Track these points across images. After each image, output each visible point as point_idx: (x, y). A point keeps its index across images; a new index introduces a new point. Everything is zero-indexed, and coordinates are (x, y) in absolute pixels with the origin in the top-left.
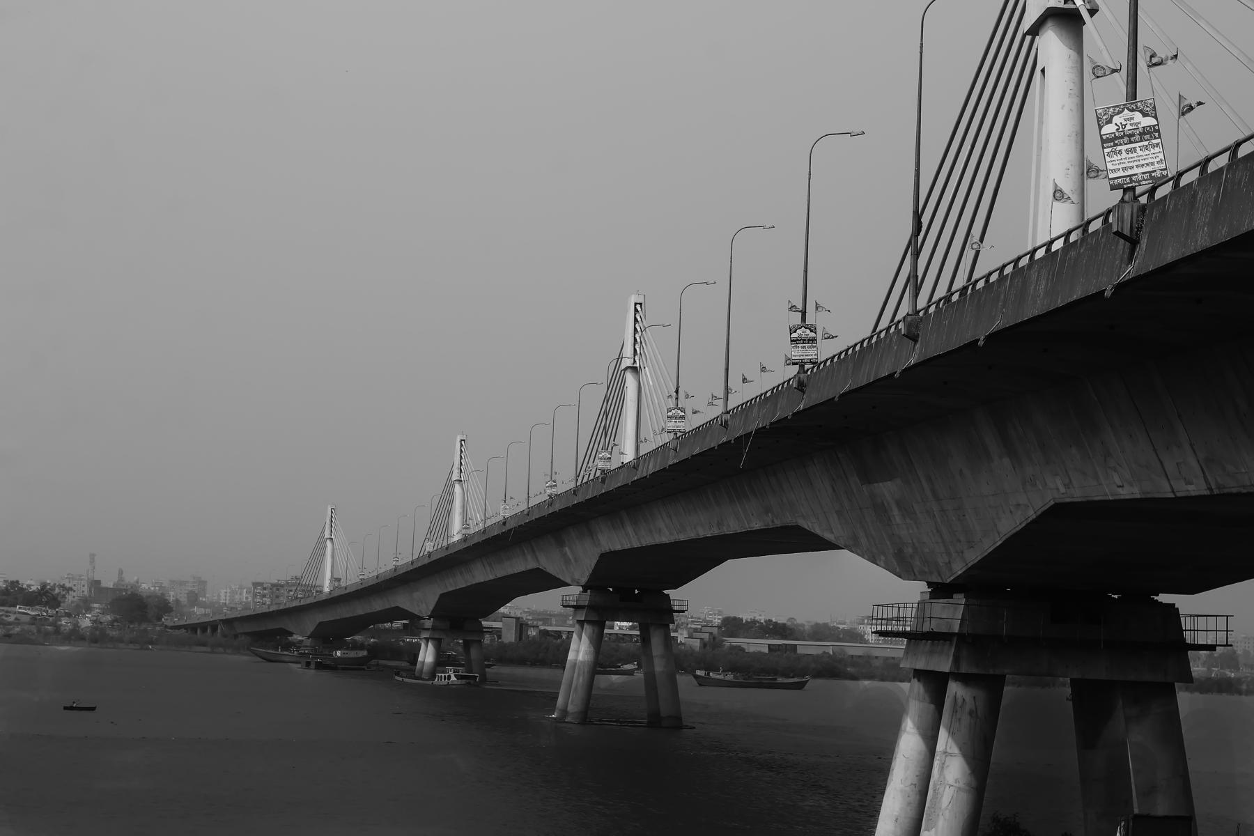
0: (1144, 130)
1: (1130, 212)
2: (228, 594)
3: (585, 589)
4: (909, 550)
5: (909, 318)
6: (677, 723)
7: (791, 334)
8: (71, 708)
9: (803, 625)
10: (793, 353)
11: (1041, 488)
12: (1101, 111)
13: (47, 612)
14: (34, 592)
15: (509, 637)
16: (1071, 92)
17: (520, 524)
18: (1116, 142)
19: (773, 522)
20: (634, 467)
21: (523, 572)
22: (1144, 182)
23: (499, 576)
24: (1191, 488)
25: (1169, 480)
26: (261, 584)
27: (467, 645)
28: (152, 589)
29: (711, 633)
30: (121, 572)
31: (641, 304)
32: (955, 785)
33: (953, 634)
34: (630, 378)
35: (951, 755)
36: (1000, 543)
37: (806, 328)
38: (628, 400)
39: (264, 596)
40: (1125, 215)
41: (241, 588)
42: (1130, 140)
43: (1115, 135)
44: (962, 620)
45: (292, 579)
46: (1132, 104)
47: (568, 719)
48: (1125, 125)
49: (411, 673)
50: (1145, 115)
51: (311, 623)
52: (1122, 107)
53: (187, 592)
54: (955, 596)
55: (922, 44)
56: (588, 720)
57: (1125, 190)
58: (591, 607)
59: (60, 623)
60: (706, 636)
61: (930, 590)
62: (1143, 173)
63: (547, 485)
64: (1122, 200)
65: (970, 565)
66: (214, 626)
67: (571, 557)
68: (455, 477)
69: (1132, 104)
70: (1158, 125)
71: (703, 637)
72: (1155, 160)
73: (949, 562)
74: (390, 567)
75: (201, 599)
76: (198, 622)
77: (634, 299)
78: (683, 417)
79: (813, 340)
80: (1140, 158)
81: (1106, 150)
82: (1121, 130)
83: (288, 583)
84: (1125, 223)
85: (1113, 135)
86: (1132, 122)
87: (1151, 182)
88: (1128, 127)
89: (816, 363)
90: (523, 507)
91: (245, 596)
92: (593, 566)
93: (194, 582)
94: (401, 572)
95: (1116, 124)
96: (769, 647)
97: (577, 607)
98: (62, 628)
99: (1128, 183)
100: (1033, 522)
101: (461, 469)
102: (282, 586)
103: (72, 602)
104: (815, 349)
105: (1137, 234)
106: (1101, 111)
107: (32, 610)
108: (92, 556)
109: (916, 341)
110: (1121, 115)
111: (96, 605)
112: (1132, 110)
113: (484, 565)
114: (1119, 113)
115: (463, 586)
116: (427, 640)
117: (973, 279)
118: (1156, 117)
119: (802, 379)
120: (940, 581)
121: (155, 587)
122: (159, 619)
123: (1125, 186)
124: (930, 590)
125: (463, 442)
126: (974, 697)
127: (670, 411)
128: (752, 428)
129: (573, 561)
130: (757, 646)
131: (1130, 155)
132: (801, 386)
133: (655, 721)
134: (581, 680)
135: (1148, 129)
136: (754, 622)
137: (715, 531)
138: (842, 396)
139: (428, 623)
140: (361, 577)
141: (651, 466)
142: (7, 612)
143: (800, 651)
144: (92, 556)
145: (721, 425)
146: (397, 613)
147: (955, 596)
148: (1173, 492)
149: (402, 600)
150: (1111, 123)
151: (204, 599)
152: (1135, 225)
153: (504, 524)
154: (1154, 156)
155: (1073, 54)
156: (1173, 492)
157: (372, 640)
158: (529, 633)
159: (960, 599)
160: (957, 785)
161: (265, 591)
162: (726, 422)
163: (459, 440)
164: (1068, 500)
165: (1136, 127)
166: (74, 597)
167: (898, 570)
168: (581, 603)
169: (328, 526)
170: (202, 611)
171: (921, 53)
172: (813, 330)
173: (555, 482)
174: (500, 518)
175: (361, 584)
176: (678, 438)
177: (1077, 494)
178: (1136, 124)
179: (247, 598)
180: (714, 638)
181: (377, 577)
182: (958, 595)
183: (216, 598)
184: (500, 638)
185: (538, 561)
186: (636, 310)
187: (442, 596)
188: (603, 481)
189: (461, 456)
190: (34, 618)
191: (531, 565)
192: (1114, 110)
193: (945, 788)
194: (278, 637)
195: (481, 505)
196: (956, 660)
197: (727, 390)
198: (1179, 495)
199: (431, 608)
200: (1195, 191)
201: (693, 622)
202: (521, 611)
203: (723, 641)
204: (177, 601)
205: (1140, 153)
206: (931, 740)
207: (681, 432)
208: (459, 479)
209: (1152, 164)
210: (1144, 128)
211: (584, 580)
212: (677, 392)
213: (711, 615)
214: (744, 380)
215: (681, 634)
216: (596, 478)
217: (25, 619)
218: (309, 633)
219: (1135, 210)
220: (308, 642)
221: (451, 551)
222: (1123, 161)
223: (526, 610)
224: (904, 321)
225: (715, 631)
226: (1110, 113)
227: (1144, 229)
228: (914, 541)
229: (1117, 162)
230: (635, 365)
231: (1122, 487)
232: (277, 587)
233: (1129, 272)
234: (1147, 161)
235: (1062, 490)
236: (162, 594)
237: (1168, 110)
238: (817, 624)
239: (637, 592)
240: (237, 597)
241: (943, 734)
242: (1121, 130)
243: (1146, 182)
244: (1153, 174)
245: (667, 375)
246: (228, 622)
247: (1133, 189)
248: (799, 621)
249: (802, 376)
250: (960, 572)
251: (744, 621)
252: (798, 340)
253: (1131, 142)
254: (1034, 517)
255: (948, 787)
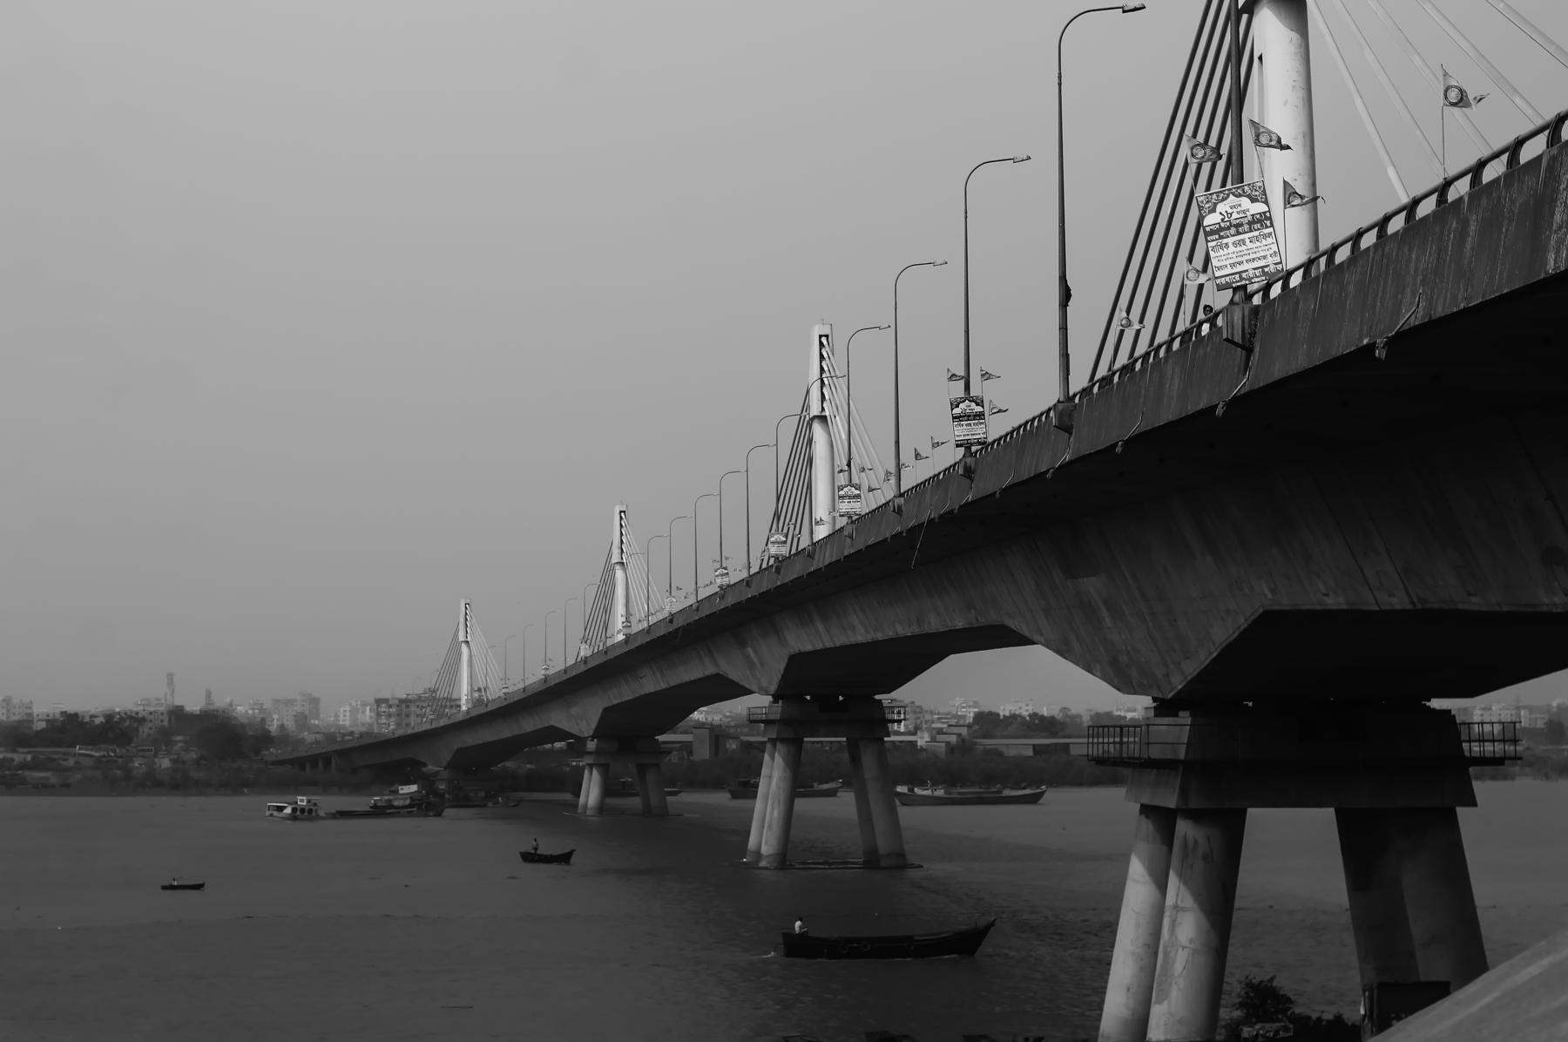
0: (1253, 218)
1: (1241, 316)
2: (348, 714)
3: (776, 698)
4: (1124, 659)
5: (1060, 407)
6: (900, 863)
7: (952, 409)
8: (172, 887)
9: (1079, 716)
10: (956, 433)
11: (1247, 591)
12: (1202, 198)
13: (115, 751)
14: (98, 726)
15: (703, 753)
16: (1294, 83)
17: (688, 622)
18: (1222, 234)
19: (977, 620)
20: (809, 555)
21: (701, 679)
22: (1256, 280)
23: (673, 684)
24: (1394, 600)
25: (1371, 591)
26: (386, 701)
27: (642, 770)
28: (250, 712)
29: (959, 735)
30: (209, 694)
31: (827, 336)
32: (1188, 945)
33: (1180, 761)
34: (817, 428)
35: (1183, 910)
36: (1215, 654)
37: (971, 401)
38: (818, 461)
39: (390, 715)
40: (1236, 318)
41: (364, 705)
42: (1237, 231)
43: (1220, 226)
44: (1189, 745)
45: (425, 693)
46: (1238, 188)
47: (763, 864)
48: (1231, 214)
49: (576, 813)
50: (1254, 200)
51: (446, 751)
52: (1226, 192)
53: (294, 713)
54: (1181, 714)
55: (1060, 74)
56: (788, 863)
57: (1235, 290)
58: (784, 721)
59: (131, 765)
60: (953, 739)
61: (1155, 704)
62: (1254, 269)
63: (717, 573)
64: (1232, 302)
65: (1189, 678)
66: (326, 759)
67: (755, 660)
68: (615, 558)
69: (1238, 188)
70: (1269, 211)
71: (960, 732)
72: (1268, 253)
73: (1168, 675)
74: (540, 674)
75: (312, 722)
76: (306, 754)
77: (818, 330)
78: (858, 496)
79: (980, 416)
80: (1250, 251)
81: (1210, 244)
82: (1226, 219)
83: (420, 697)
84: (1236, 327)
85: (1217, 226)
86: (1239, 209)
87: (1264, 278)
88: (1235, 216)
89: (985, 442)
90: (692, 600)
91: (367, 716)
92: (782, 671)
93: (303, 701)
94: (553, 683)
95: (1221, 213)
96: (1034, 750)
97: (767, 722)
98: (135, 772)
99: (1237, 282)
100: (1246, 630)
101: (622, 549)
102: (410, 701)
103: (149, 735)
104: (983, 426)
105: (1250, 340)
106: (1202, 198)
107: (96, 751)
108: (170, 677)
109: (1070, 434)
110: (1224, 202)
111: (179, 738)
112: (1239, 196)
113: (653, 672)
114: (1224, 199)
115: (630, 698)
116: (591, 766)
117: (1156, 344)
118: (1266, 202)
119: (968, 465)
120: (1161, 696)
121: (254, 709)
122: (257, 752)
123: (1234, 285)
124: (1155, 704)
125: (623, 515)
126: (1209, 838)
127: (957, 406)
128: (925, 518)
129: (757, 664)
130: (1020, 747)
131: (1239, 249)
132: (969, 473)
133: (872, 861)
134: (776, 813)
135: (1258, 216)
136: (1014, 717)
137: (914, 630)
138: (1004, 491)
139: (591, 745)
140: (504, 691)
141: (827, 554)
142: (64, 754)
143: (1074, 751)
144: (170, 677)
145: (894, 511)
146: (555, 734)
147: (1181, 714)
148: (1377, 604)
149: (558, 718)
150: (1215, 212)
151: (317, 722)
152: (1247, 330)
153: (671, 621)
154: (1266, 248)
155: (1295, 36)
156: (1377, 604)
157: (529, 766)
158: (728, 746)
159: (1185, 718)
160: (1192, 946)
161: (391, 710)
162: (899, 507)
163: (618, 512)
164: (1277, 608)
165: (1244, 215)
166: (151, 728)
167: (1116, 681)
168: (772, 717)
169: (462, 626)
170: (313, 736)
171: (1060, 84)
172: (980, 403)
173: (725, 569)
174: (665, 614)
175: (505, 699)
176: (852, 522)
177: (1285, 602)
178: (1244, 212)
179: (371, 717)
180: (963, 741)
181: (524, 690)
182: (1185, 712)
183: (332, 719)
184: (691, 755)
185: (717, 665)
186: (821, 344)
187: (605, 710)
188: (778, 570)
189: (621, 532)
190: (99, 760)
191: (710, 670)
192: (1218, 196)
193: (1177, 950)
194: (409, 769)
195: (644, 595)
196: (1184, 794)
197: (899, 467)
198: (1383, 608)
199: (594, 726)
200: (1298, 299)
201: (939, 718)
202: (721, 716)
203: (976, 743)
204: (282, 727)
205: (1250, 245)
206: (1162, 887)
207: (857, 515)
208: (620, 560)
209: (1265, 257)
210: (1253, 215)
211: (773, 688)
212: (849, 465)
213: (964, 707)
214: (917, 456)
215: (922, 738)
216: (769, 567)
217: (88, 762)
218: (445, 763)
219: (1247, 313)
220: (445, 774)
221: (611, 656)
222: (1231, 256)
223: (728, 714)
224: (1055, 410)
225: (964, 731)
226: (1213, 201)
227: (1257, 335)
228: (1129, 648)
229: (1224, 258)
230: (823, 414)
231: (1327, 595)
232: (405, 702)
233: (1243, 385)
234: (1258, 255)
235: (1269, 595)
236: (263, 720)
237: (865, 487)
238: (1098, 715)
239: (841, 698)
240: (360, 716)
241: (1173, 881)
242: (1226, 219)
243: (1259, 279)
244: (1266, 270)
245: (863, 429)
246: (344, 753)
247: (1244, 287)
248: (1074, 711)
249: (969, 460)
250: (1180, 687)
251: (1002, 717)
252: (1222, 229)
253: (1239, 233)
254: (1246, 625)
255: (1180, 949)
